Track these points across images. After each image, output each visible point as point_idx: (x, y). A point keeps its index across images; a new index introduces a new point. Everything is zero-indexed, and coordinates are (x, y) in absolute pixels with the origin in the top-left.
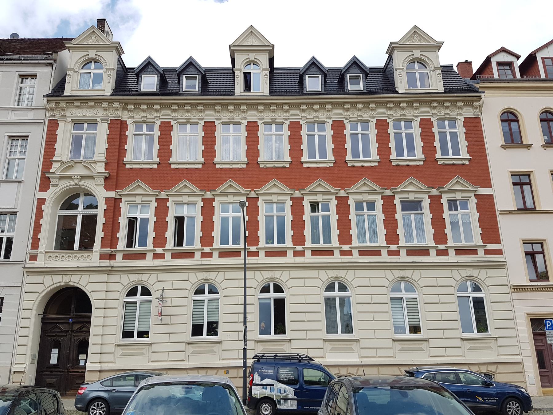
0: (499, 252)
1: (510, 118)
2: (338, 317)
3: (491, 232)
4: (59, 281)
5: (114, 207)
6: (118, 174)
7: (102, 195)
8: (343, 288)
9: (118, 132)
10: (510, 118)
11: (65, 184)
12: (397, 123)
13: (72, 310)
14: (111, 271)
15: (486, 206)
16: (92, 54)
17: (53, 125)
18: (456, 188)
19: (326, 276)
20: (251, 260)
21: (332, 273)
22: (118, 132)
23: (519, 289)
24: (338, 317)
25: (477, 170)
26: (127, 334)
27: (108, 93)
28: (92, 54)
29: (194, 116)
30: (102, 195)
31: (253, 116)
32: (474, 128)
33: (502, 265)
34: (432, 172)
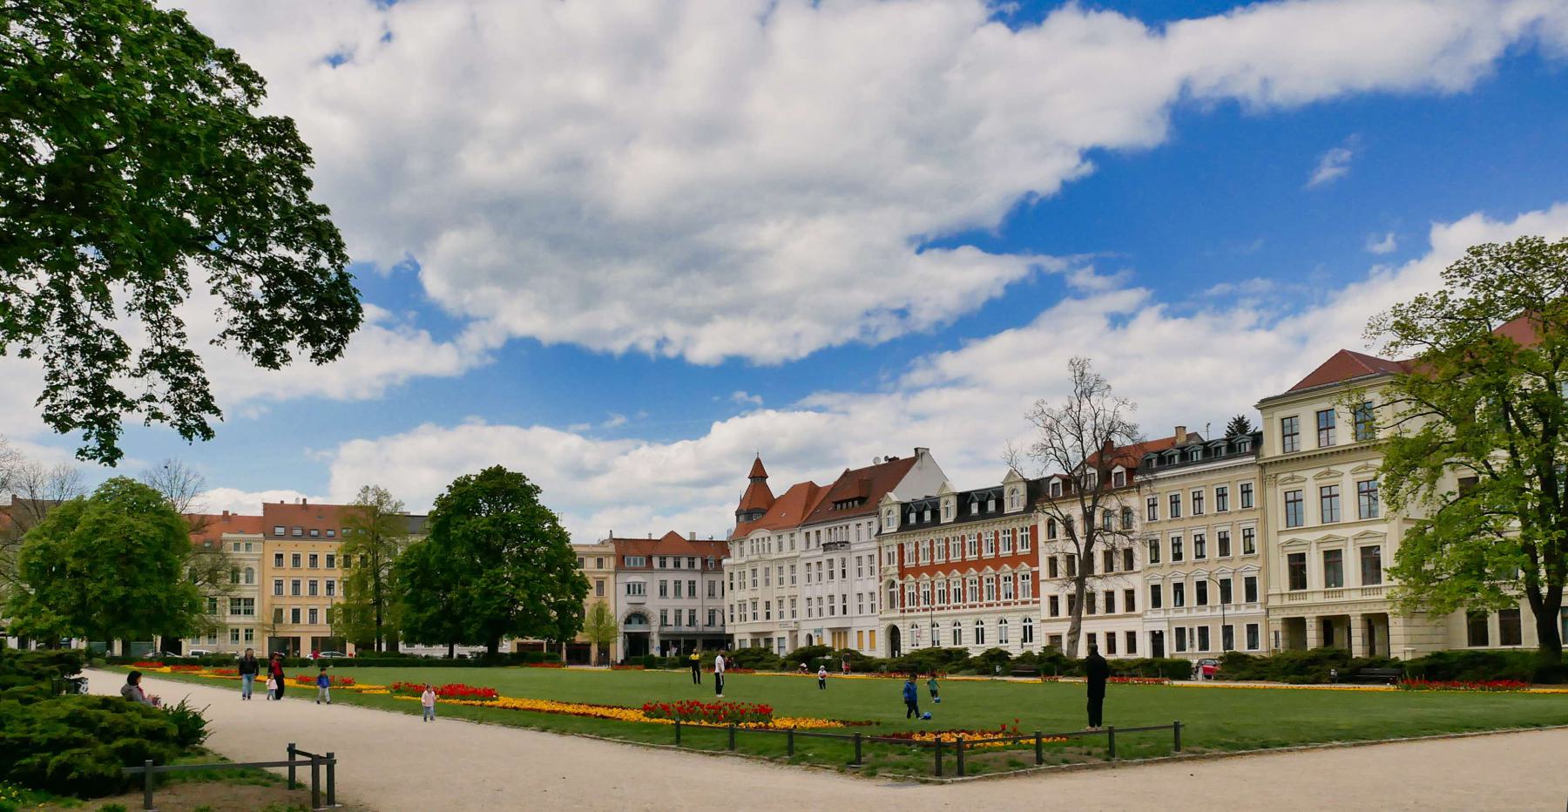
3: (1036, 593)
6: (903, 573)
7: (898, 582)
9: (901, 547)
15: (1035, 575)
19: (1022, 615)
22: (901, 547)
25: (1033, 559)
27: (1021, 508)
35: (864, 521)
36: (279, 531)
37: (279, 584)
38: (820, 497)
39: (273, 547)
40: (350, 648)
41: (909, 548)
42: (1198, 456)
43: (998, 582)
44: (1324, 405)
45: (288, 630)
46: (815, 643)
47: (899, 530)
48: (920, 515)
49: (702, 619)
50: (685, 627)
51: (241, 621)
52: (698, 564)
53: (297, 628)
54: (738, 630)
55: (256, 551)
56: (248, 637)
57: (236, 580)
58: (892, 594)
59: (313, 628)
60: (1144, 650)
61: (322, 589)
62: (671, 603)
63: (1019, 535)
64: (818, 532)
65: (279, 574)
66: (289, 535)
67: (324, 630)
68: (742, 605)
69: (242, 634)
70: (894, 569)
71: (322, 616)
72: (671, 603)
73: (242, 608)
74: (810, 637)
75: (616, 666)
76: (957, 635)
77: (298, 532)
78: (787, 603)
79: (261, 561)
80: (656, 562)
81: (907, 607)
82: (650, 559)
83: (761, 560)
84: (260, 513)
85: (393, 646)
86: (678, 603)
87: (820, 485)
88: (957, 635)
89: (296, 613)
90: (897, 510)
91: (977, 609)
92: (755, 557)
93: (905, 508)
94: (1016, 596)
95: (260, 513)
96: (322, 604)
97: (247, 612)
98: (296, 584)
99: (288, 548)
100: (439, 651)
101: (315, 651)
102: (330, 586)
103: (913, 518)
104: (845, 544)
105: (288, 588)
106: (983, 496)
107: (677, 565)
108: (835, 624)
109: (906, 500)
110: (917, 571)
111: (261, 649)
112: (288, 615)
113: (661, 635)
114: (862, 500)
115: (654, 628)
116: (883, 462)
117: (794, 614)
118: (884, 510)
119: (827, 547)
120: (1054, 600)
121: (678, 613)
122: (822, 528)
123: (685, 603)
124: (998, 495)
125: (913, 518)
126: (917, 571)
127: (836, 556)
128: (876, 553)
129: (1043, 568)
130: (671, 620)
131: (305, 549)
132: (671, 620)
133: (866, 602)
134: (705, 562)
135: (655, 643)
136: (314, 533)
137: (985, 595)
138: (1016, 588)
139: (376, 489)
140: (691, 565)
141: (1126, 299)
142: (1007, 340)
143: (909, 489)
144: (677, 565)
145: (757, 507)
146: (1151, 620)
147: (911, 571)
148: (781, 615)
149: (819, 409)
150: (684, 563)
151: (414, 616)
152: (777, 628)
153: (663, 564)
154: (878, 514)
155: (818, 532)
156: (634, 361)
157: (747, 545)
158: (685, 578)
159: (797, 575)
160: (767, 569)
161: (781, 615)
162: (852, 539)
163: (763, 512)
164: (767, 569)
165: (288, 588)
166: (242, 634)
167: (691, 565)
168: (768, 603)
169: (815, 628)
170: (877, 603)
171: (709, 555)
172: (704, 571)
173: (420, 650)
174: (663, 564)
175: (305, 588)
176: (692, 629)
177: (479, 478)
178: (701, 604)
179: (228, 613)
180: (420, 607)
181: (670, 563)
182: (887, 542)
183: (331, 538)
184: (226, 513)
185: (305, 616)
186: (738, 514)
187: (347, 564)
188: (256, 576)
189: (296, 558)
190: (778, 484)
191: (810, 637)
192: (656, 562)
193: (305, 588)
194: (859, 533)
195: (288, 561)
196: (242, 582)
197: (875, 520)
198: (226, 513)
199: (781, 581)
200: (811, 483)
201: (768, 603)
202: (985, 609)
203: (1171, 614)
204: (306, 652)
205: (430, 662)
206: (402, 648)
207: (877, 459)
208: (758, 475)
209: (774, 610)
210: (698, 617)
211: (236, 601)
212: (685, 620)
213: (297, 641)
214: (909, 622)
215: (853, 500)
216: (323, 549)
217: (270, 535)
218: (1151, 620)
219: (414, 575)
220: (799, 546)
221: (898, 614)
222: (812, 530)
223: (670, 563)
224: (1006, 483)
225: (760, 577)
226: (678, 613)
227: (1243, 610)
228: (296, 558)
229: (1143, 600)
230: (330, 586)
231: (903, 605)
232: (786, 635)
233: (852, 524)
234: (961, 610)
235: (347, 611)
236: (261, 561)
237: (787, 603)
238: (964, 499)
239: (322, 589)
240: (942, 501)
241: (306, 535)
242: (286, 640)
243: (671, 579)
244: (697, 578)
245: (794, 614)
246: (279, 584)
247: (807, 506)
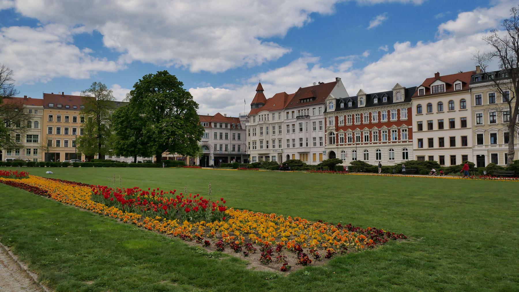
0: (412, 142)
1: (419, 107)
2: (379, 156)
3: (411, 137)
4: (330, 150)
5: (337, 134)
6: (337, 129)
7: (335, 133)
8: (380, 151)
9: (337, 118)
10: (419, 107)
11: (329, 131)
12: (365, 114)
13: (213, 158)
14: (338, 148)
15: (410, 130)
16: (398, 91)
17: (326, 118)
18: (405, 126)
19: (376, 148)
20: (357, 146)
21: (390, 147)
22: (337, 118)
23: (414, 150)
24: (379, 156)
25: (409, 122)
26: (390, 159)
27: (403, 100)
28: (398, 91)
29: (342, 114)
30: (335, 133)
31: (399, 107)
32: (410, 110)
33: (412, 145)
34: (399, 123)
35: (317, 107)
36: (51, 105)
37: (50, 129)
38: (290, 100)
39: (48, 112)
40: (83, 158)
41: (341, 119)
42: (480, 79)
43: (389, 133)
44: (293, 110)
45: (54, 150)
46: (291, 158)
47: (336, 110)
48: (347, 104)
49: (230, 148)
50: (223, 152)
51: (32, 145)
52: (229, 127)
53: (58, 149)
54: (252, 153)
55: (40, 114)
56: (35, 152)
57: (29, 126)
58: (331, 138)
59: (66, 149)
60: (448, 163)
61: (70, 131)
62: (219, 142)
63: (355, 117)
64: (293, 112)
65: (51, 125)
66: (55, 107)
67: (72, 150)
68: (255, 142)
69: (32, 151)
70: (333, 127)
71: (70, 144)
72: (219, 142)
73: (32, 139)
74: (288, 156)
75: (212, 166)
76: (366, 156)
77: (60, 106)
78: (277, 142)
79: (42, 118)
80: (213, 125)
81: (339, 143)
82: (210, 123)
83: (265, 123)
84: (41, 97)
85: (101, 157)
86: (221, 142)
87: (288, 93)
88: (366, 156)
89: (58, 142)
90: (334, 102)
91: (378, 144)
92: (263, 122)
93: (338, 102)
94: (399, 139)
95: (41, 97)
96: (71, 138)
97: (35, 141)
98: (58, 129)
99: (55, 113)
100: (130, 160)
101: (67, 158)
102: (74, 130)
103: (342, 105)
104: (308, 116)
105: (54, 131)
106: (380, 96)
107: (221, 126)
108: (302, 150)
109: (338, 98)
110: (345, 128)
111: (41, 158)
112: (54, 143)
113: (214, 154)
114: (314, 98)
115: (212, 152)
116: (317, 84)
117: (280, 146)
118: (328, 102)
119: (298, 118)
120: (420, 141)
121: (221, 146)
122: (296, 111)
123: (224, 142)
124: (389, 95)
125: (342, 105)
126: (345, 128)
127: (303, 122)
128: (323, 121)
129: (415, 127)
130: (218, 148)
131: (63, 114)
132: (218, 148)
133: (318, 141)
134: (231, 126)
135: (212, 157)
136: (67, 107)
137: (373, 139)
138: (399, 135)
139: (100, 84)
140: (226, 126)
141: (314, 60)
142: (281, 71)
143: (334, 95)
144: (221, 126)
145: (260, 103)
146: (478, 150)
147: (342, 128)
148: (274, 146)
149: (226, 88)
150: (224, 126)
151: (122, 142)
152: (272, 152)
153: (215, 126)
154: (324, 104)
155: (293, 112)
156: (17, 166)
157: (257, 118)
158: (224, 132)
159: (282, 130)
160: (267, 128)
161: (274, 146)
162: (311, 114)
163: (264, 105)
164: (267, 128)
165: (54, 131)
166: (32, 151)
167: (226, 126)
168: (267, 141)
169: (294, 153)
170: (323, 141)
171: (234, 123)
172: (231, 129)
173: (122, 159)
174: (215, 126)
175: (62, 131)
176: (226, 152)
177: (157, 76)
178: (230, 142)
179: (25, 141)
180: (125, 137)
181: (218, 125)
182: (329, 116)
183: (75, 109)
184: (25, 97)
185: (62, 144)
186: (252, 105)
187: (82, 121)
188: (39, 125)
189: (59, 117)
190: (268, 94)
191: (288, 156)
192: (213, 125)
193: (62, 131)
194: (316, 112)
195: (55, 119)
196: (33, 127)
197: (323, 107)
198: (25, 97)
199: (274, 132)
200: (285, 93)
201: (267, 141)
202: (347, 146)
203: (490, 147)
204: (62, 159)
205: (124, 165)
206: (107, 157)
207: (314, 83)
208: (260, 90)
209: (271, 144)
210: (229, 147)
211: (29, 136)
212: (224, 149)
213: (58, 155)
214: (340, 150)
215: (309, 98)
216: (72, 114)
217: (46, 107)
218: (478, 150)
219: (122, 122)
220: (281, 117)
221: (335, 146)
222: (290, 111)
223: (218, 125)
224: (394, 89)
225: (264, 130)
226: (221, 146)
227: (490, 147)
228: (59, 117)
229: (472, 141)
230: (74, 130)
231: (337, 142)
232: (276, 155)
233: (311, 108)
234: (344, 146)
235: (83, 141)
236: (42, 118)
237: (277, 142)
238: (370, 98)
239: (70, 131)
240: (359, 98)
241: (63, 108)
242: (53, 154)
243: (218, 132)
244: (229, 132)
245: (280, 146)
246: (50, 129)
247: (285, 102)
